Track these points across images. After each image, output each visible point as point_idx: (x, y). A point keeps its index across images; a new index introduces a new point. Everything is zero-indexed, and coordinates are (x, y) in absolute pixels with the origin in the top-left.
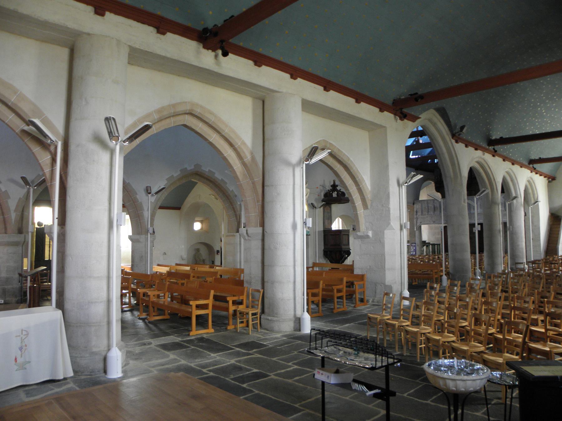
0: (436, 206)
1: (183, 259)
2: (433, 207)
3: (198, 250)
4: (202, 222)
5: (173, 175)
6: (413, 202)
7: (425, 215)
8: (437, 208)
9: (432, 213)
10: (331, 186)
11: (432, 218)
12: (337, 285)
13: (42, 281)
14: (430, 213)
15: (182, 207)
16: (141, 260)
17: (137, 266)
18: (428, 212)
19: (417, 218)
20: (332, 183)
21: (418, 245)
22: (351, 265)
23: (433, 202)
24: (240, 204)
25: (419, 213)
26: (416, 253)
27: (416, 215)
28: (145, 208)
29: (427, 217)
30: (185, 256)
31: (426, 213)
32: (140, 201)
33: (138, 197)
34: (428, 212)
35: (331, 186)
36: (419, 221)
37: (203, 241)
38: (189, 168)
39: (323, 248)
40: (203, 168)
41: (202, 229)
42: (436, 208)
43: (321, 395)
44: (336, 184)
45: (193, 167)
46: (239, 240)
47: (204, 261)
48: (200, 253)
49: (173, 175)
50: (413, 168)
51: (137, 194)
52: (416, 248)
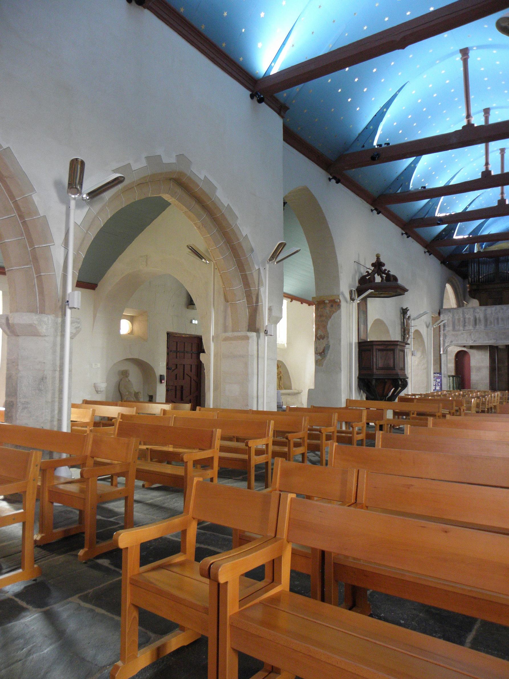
0: (477, 317)
1: (97, 392)
2: (472, 318)
3: (124, 374)
4: (132, 319)
5: (129, 164)
6: (438, 311)
7: (459, 330)
8: (480, 320)
9: (471, 328)
10: (373, 265)
11: (470, 335)
12: (294, 432)
13: (473, 282)
14: (467, 328)
15: (99, 285)
16: (40, 390)
17: (24, 408)
18: (464, 326)
19: (445, 336)
20: (374, 260)
21: (445, 377)
22: (155, 401)
23: (474, 311)
24: (259, 269)
25: (449, 328)
26: (441, 388)
27: (444, 330)
28: (58, 238)
29: (462, 334)
30: (103, 386)
31: (461, 328)
32: (42, 213)
33: (36, 198)
34: (464, 326)
35: (373, 265)
36: (448, 340)
37: (136, 356)
38: (166, 160)
39: (357, 375)
40: (194, 169)
41: (132, 332)
42: (478, 321)
43: (124, 509)
44: (382, 260)
45: (173, 160)
46: (255, 347)
47: (136, 395)
48: (129, 381)
49: (129, 164)
50: (439, 259)
51: (33, 190)
52: (441, 380)
